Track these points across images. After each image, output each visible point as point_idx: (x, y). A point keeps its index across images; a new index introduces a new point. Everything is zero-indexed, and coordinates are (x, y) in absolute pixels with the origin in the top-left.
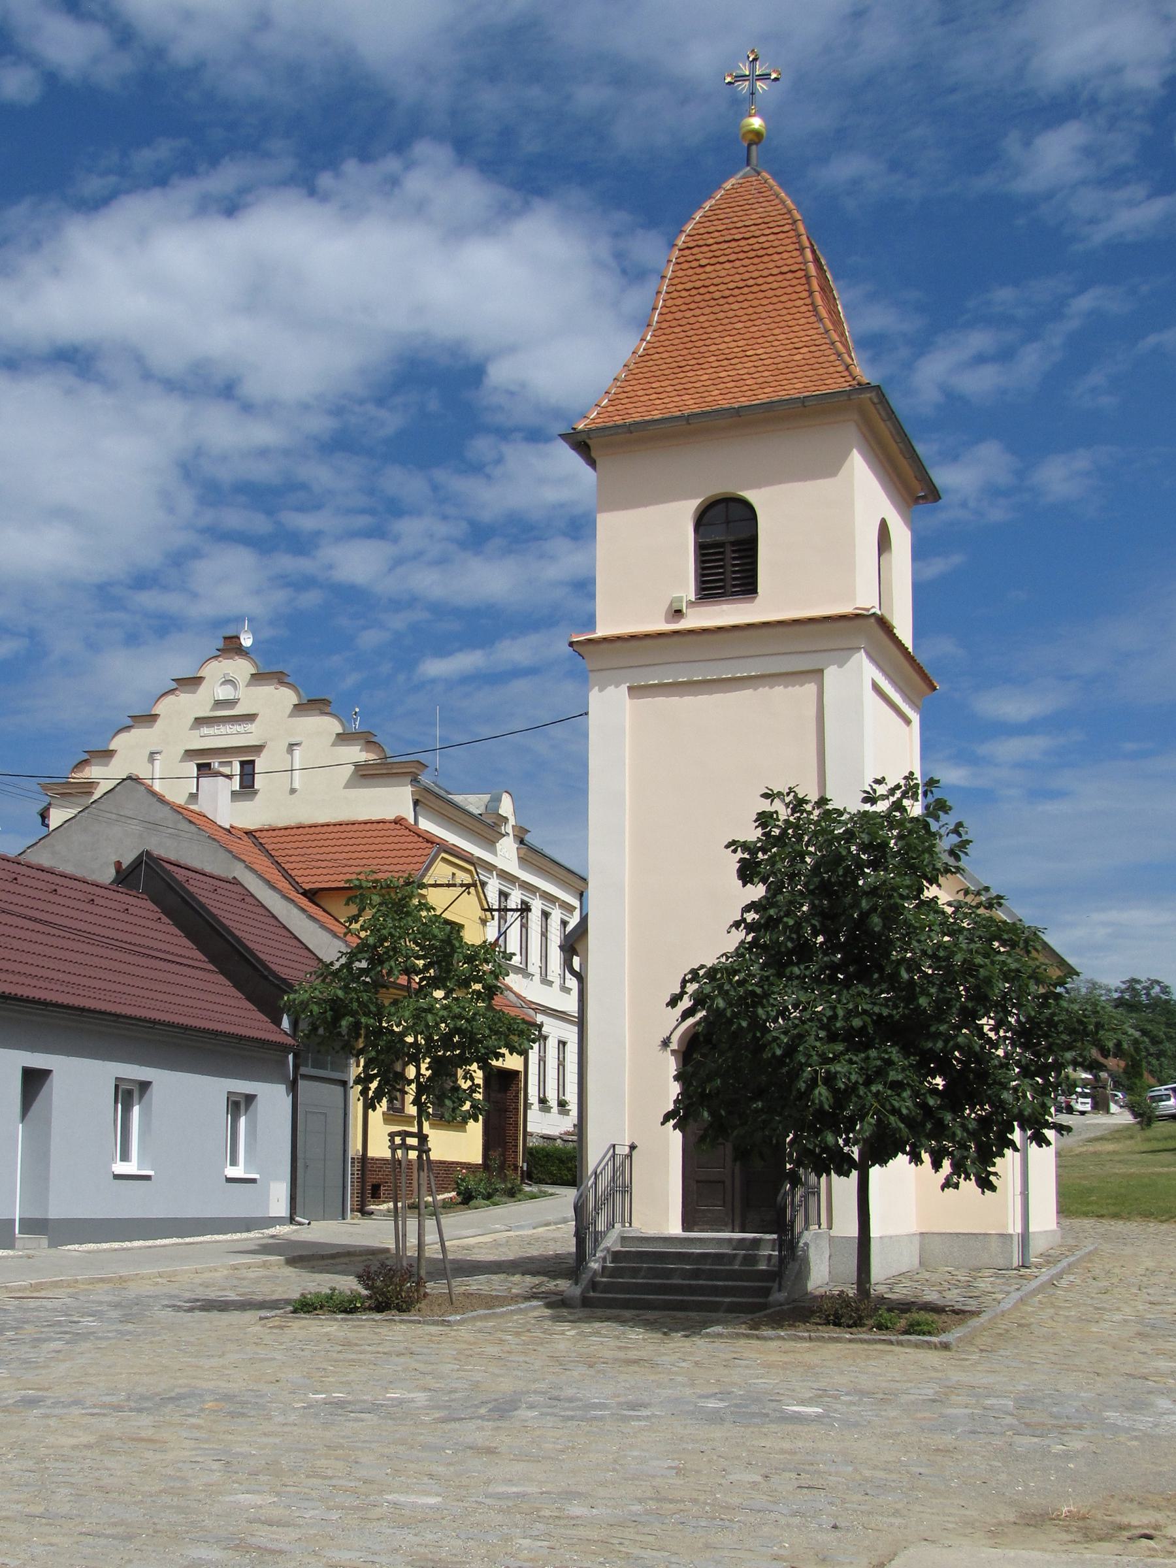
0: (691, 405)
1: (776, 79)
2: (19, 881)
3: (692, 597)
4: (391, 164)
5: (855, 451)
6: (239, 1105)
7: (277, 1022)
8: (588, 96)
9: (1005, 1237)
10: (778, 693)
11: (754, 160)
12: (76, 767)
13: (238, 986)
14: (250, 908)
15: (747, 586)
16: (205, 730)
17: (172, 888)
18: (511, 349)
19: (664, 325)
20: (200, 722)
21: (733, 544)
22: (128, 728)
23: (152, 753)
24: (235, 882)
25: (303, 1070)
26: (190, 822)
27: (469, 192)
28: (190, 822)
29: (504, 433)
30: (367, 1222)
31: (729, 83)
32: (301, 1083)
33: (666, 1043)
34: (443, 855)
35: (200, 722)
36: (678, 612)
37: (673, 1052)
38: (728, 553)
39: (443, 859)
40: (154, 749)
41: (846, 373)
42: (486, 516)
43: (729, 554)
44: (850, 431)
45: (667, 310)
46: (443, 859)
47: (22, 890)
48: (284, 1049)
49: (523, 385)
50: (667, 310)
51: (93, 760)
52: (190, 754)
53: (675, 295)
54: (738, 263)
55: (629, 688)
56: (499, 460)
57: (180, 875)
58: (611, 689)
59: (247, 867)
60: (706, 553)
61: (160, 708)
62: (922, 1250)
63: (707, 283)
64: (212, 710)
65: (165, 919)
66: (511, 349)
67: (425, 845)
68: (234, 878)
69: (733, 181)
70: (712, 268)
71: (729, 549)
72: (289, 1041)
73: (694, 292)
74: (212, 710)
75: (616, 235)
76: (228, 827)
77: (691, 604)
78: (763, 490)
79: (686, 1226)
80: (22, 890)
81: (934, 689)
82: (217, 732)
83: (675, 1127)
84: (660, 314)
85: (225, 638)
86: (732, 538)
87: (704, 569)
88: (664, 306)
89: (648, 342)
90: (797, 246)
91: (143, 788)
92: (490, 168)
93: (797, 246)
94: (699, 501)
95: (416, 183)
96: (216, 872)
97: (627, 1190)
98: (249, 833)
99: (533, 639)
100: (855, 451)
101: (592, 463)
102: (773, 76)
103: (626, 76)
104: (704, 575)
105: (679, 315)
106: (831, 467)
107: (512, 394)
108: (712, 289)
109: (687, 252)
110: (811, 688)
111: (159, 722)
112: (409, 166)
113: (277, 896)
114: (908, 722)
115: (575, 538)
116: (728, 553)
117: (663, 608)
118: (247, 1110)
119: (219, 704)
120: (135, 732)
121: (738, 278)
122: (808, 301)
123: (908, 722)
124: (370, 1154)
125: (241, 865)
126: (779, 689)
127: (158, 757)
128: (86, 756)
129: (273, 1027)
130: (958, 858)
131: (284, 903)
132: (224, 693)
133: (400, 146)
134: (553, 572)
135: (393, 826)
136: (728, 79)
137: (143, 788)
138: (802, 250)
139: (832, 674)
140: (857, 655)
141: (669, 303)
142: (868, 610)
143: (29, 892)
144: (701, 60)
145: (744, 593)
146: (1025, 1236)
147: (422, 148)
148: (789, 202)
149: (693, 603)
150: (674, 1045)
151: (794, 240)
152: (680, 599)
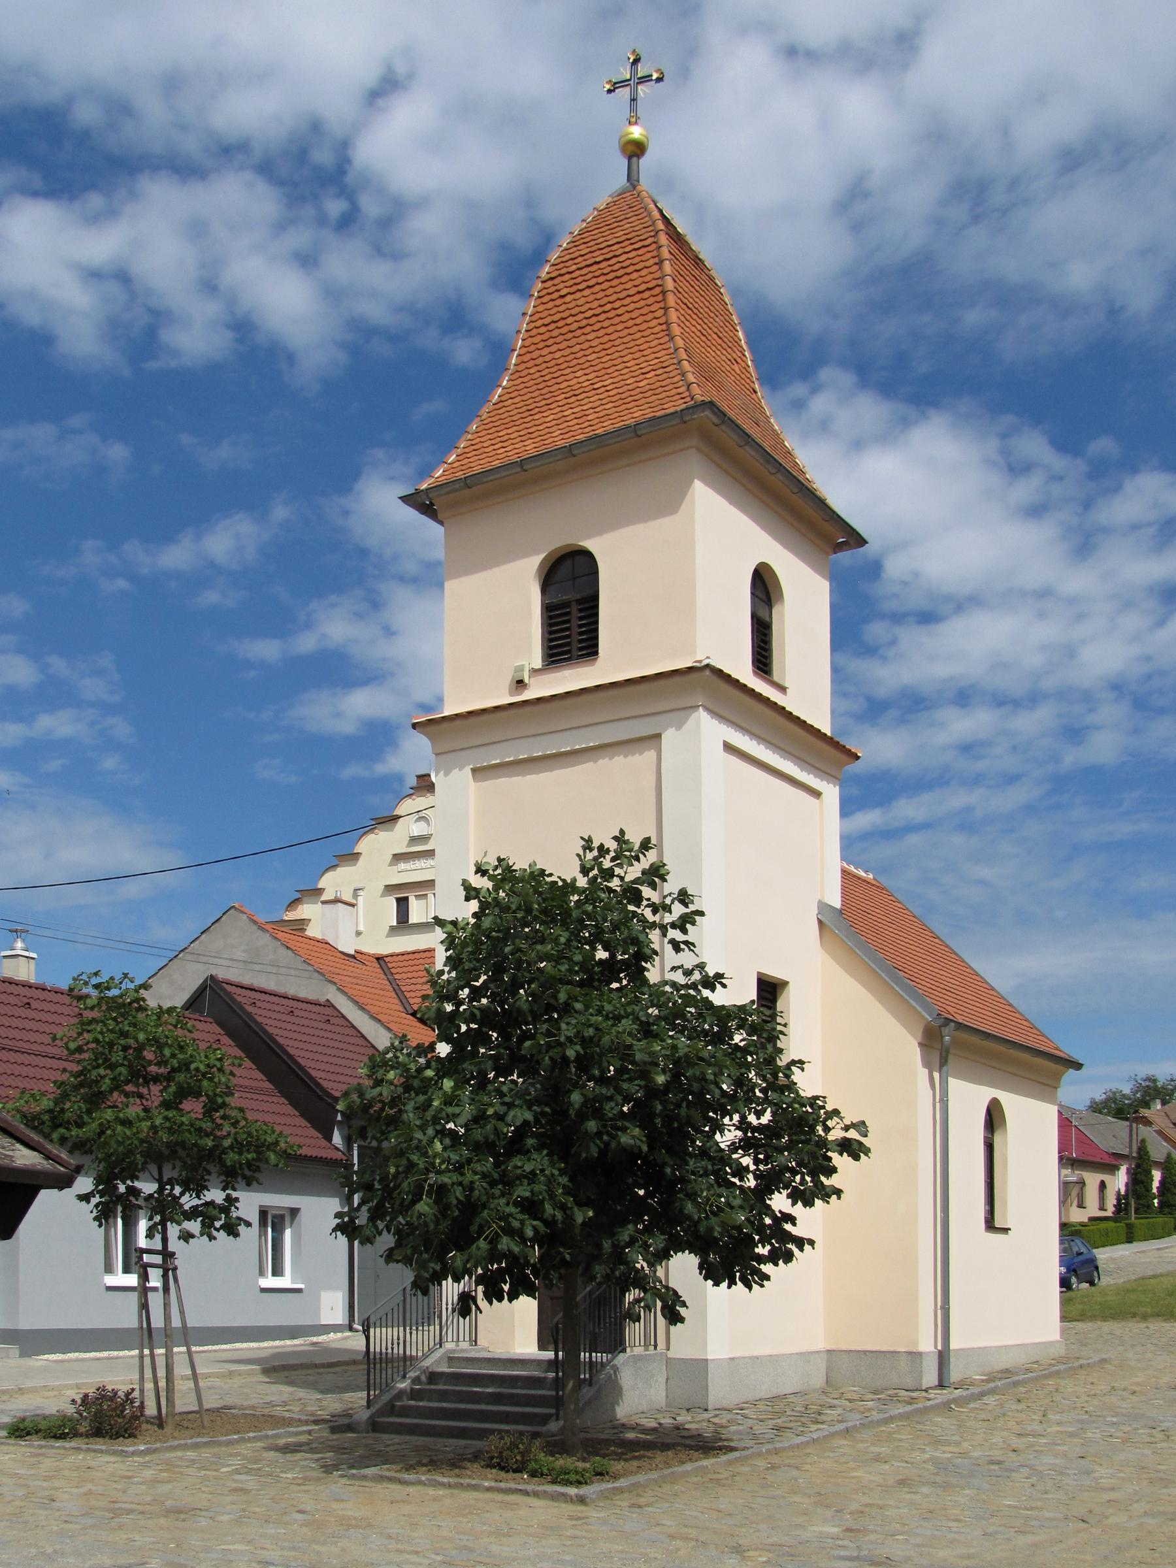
1: (659, 80)
2: (33, 1006)
3: (538, 663)
4: (799, 389)
5: (696, 481)
7: (328, 1137)
8: (973, 318)
9: (915, 1356)
10: (619, 763)
12: (289, 905)
13: (294, 1103)
14: (338, 1029)
15: (589, 648)
16: (402, 866)
17: (234, 1011)
18: (904, 545)
19: (523, 366)
20: (398, 858)
21: (579, 602)
22: (334, 867)
23: (356, 890)
24: (329, 1004)
26: (288, 948)
27: (869, 410)
28: (288, 948)
29: (898, 618)
35: (398, 858)
36: (520, 682)
38: (571, 612)
40: (359, 886)
41: (687, 394)
42: (882, 693)
43: (575, 614)
44: (693, 460)
45: (525, 350)
47: (297, 1020)
49: (916, 574)
50: (525, 350)
51: (305, 899)
52: (390, 889)
53: (535, 332)
54: (597, 288)
55: (474, 771)
56: (894, 642)
57: (242, 997)
58: (455, 772)
59: (338, 989)
60: (553, 616)
61: (361, 847)
62: (829, 1369)
64: (408, 846)
66: (904, 545)
68: (328, 1000)
70: (573, 297)
71: (574, 609)
73: (553, 326)
74: (408, 846)
75: (1004, 436)
76: (352, 952)
77: (534, 672)
78: (605, 536)
80: (297, 1020)
81: (858, 758)
82: (413, 867)
83: (389, 1257)
84: (519, 355)
85: (418, 777)
86: (578, 597)
87: (551, 633)
88: (523, 346)
89: (504, 388)
90: (656, 260)
91: (244, 917)
92: (887, 390)
93: (656, 260)
94: (542, 556)
95: (820, 404)
96: (312, 996)
98: (379, 959)
99: (926, 797)
100: (696, 481)
101: (441, 523)
102: (655, 76)
103: (1009, 298)
106: (671, 502)
107: (905, 583)
109: (550, 283)
110: (651, 755)
111: (362, 859)
112: (814, 391)
113: (365, 1017)
114: (817, 794)
115: (963, 706)
116: (571, 612)
117: (507, 679)
118: (292, 1223)
119: (414, 840)
120: (340, 870)
121: (596, 304)
122: (662, 320)
123: (817, 794)
125: (333, 988)
126: (619, 760)
127: (361, 893)
128: (298, 895)
129: (324, 1142)
130: (685, 931)
131: (373, 1023)
132: (418, 829)
133: (808, 372)
134: (940, 738)
137: (244, 917)
138: (660, 263)
139: (670, 737)
140: (694, 716)
141: (527, 343)
142: (700, 662)
143: (303, 1021)
144: (1080, 277)
145: (589, 655)
146: (943, 1357)
147: (826, 374)
149: (539, 670)
151: (655, 253)
152: (520, 669)
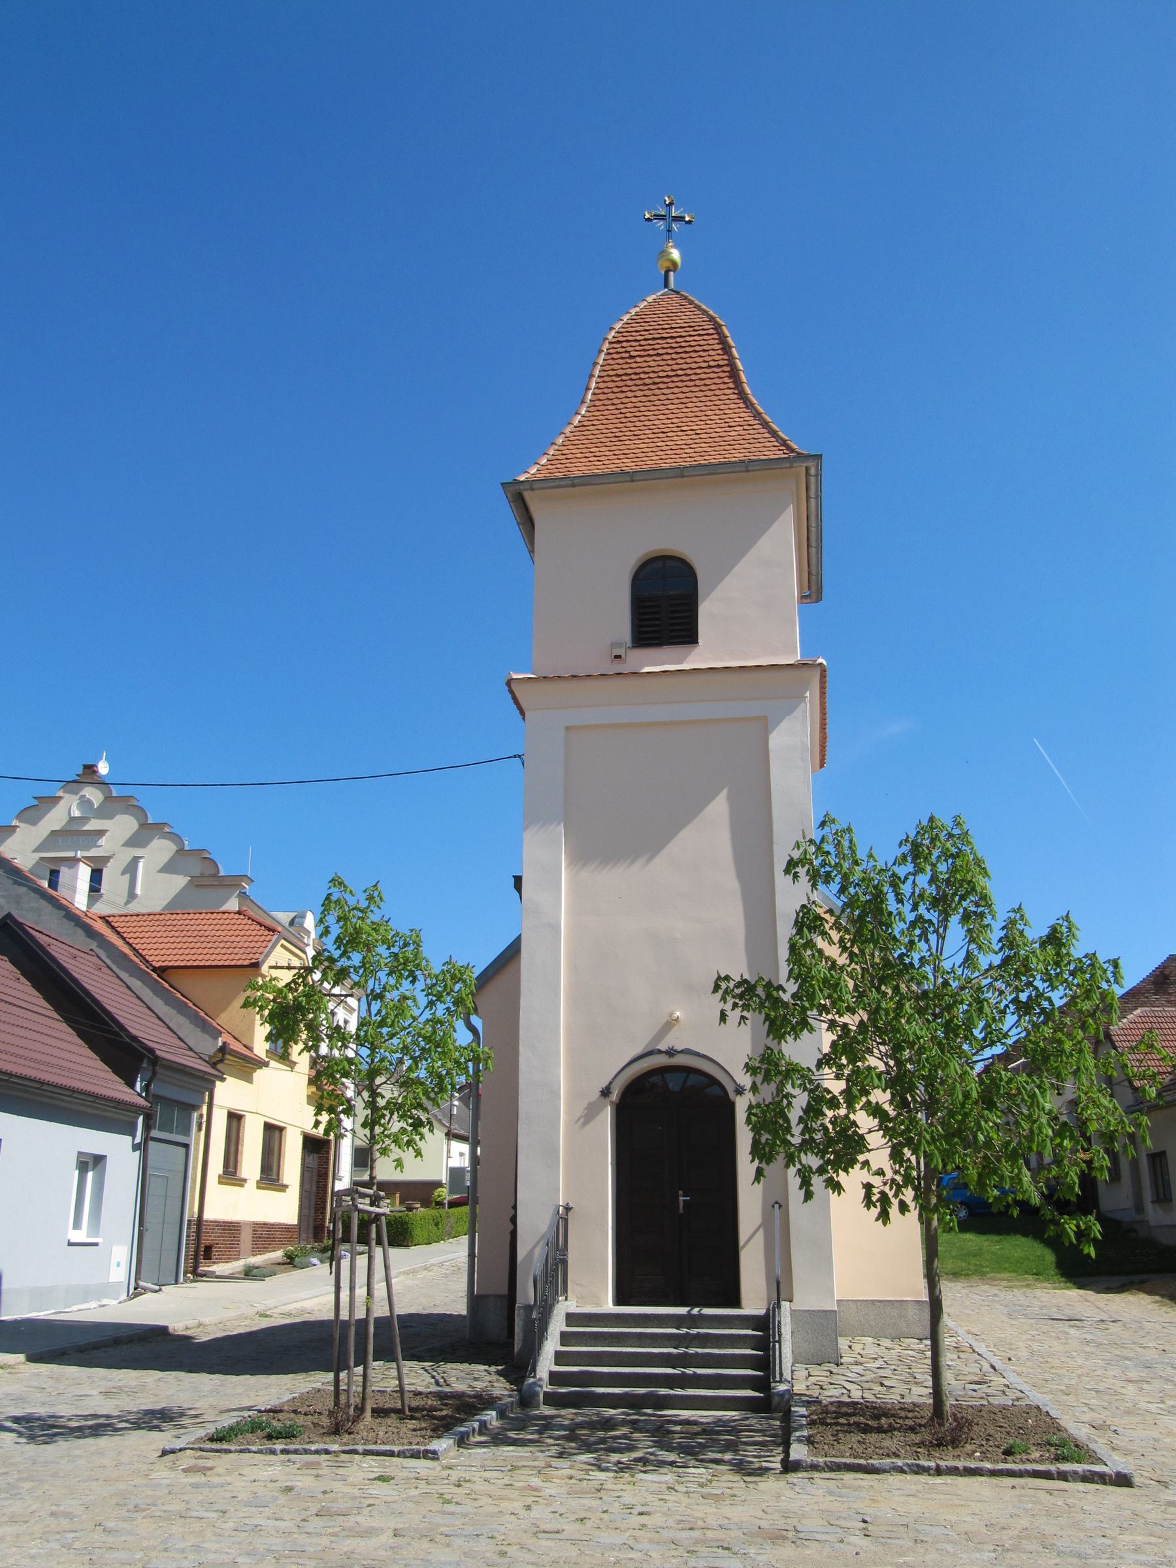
0: (631, 465)
1: (689, 222)
6: (91, 1163)
11: (672, 285)
15: (683, 631)
25: (155, 1133)
30: (202, 1289)
31: (649, 220)
32: (151, 1144)
33: (606, 1092)
34: (283, 942)
37: (612, 1103)
39: (283, 946)
46: (283, 946)
48: (136, 1109)
63: (638, 371)
65: (23, 979)
67: (267, 932)
69: (654, 297)
72: (142, 1102)
79: (619, 1300)
84: (594, 394)
97: (564, 1262)
104: (641, 626)
105: (611, 396)
108: (642, 376)
124: (207, 1216)
135: (237, 916)
136: (647, 216)
148: (711, 312)
150: (615, 1096)
